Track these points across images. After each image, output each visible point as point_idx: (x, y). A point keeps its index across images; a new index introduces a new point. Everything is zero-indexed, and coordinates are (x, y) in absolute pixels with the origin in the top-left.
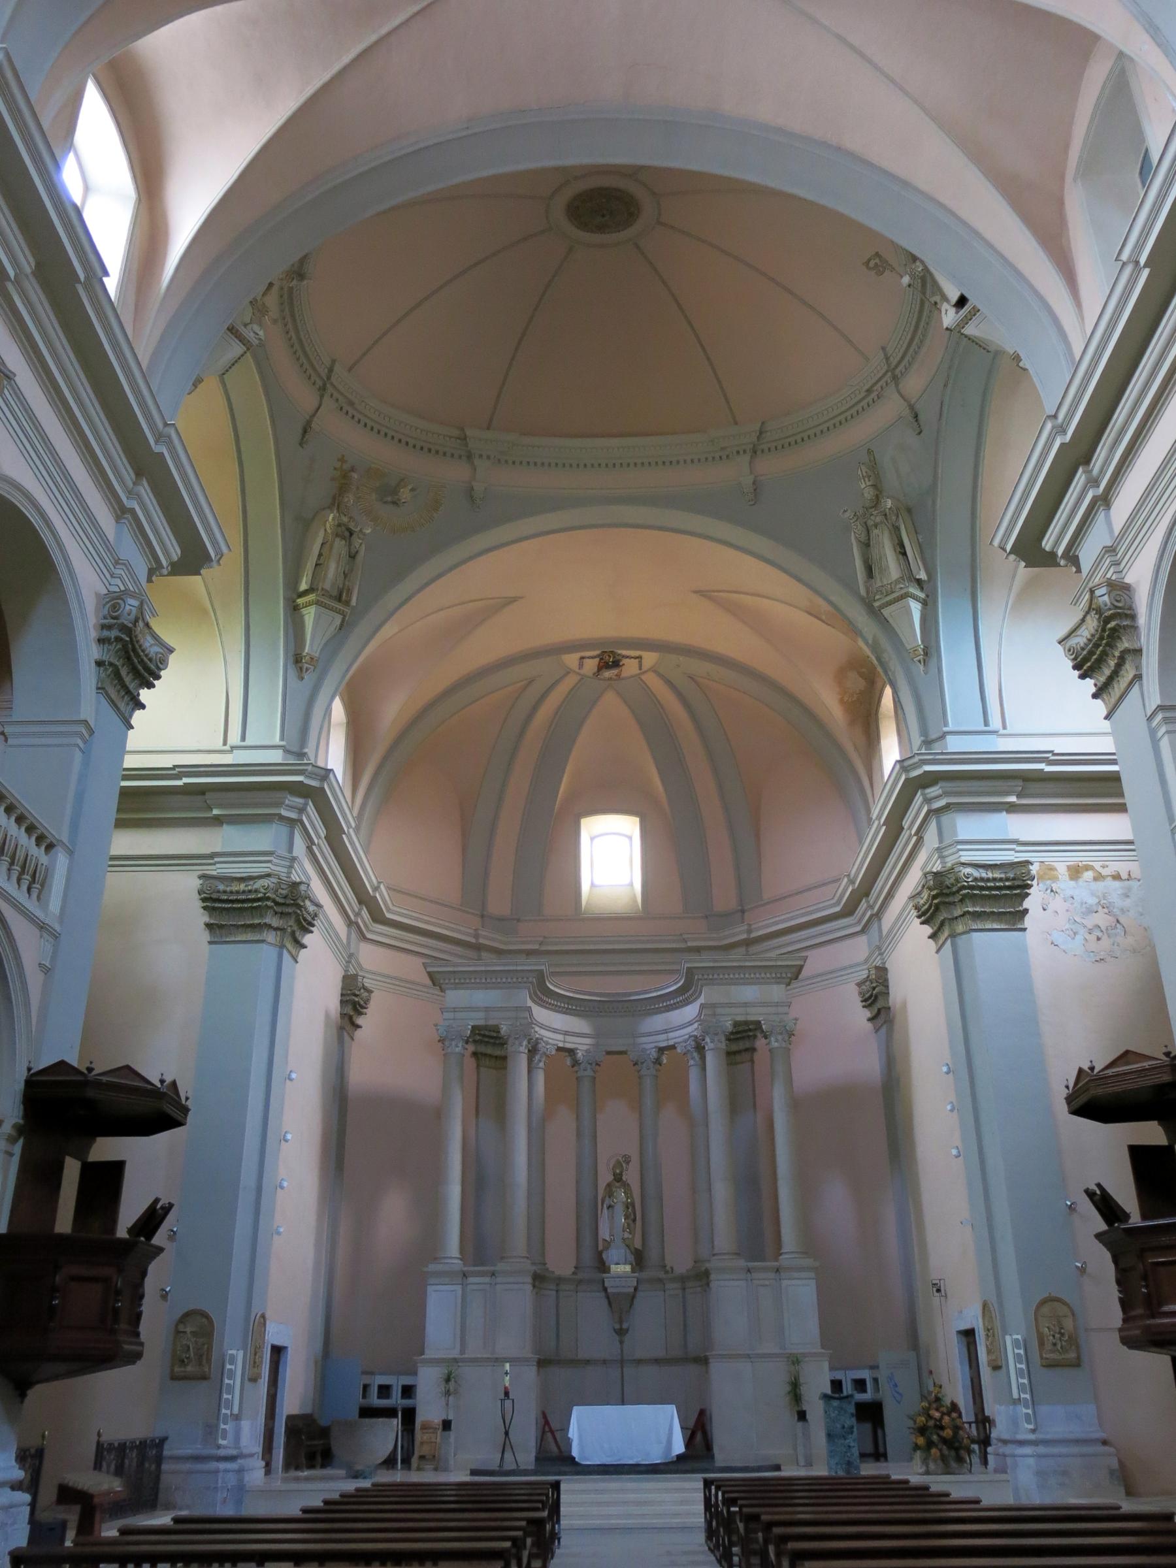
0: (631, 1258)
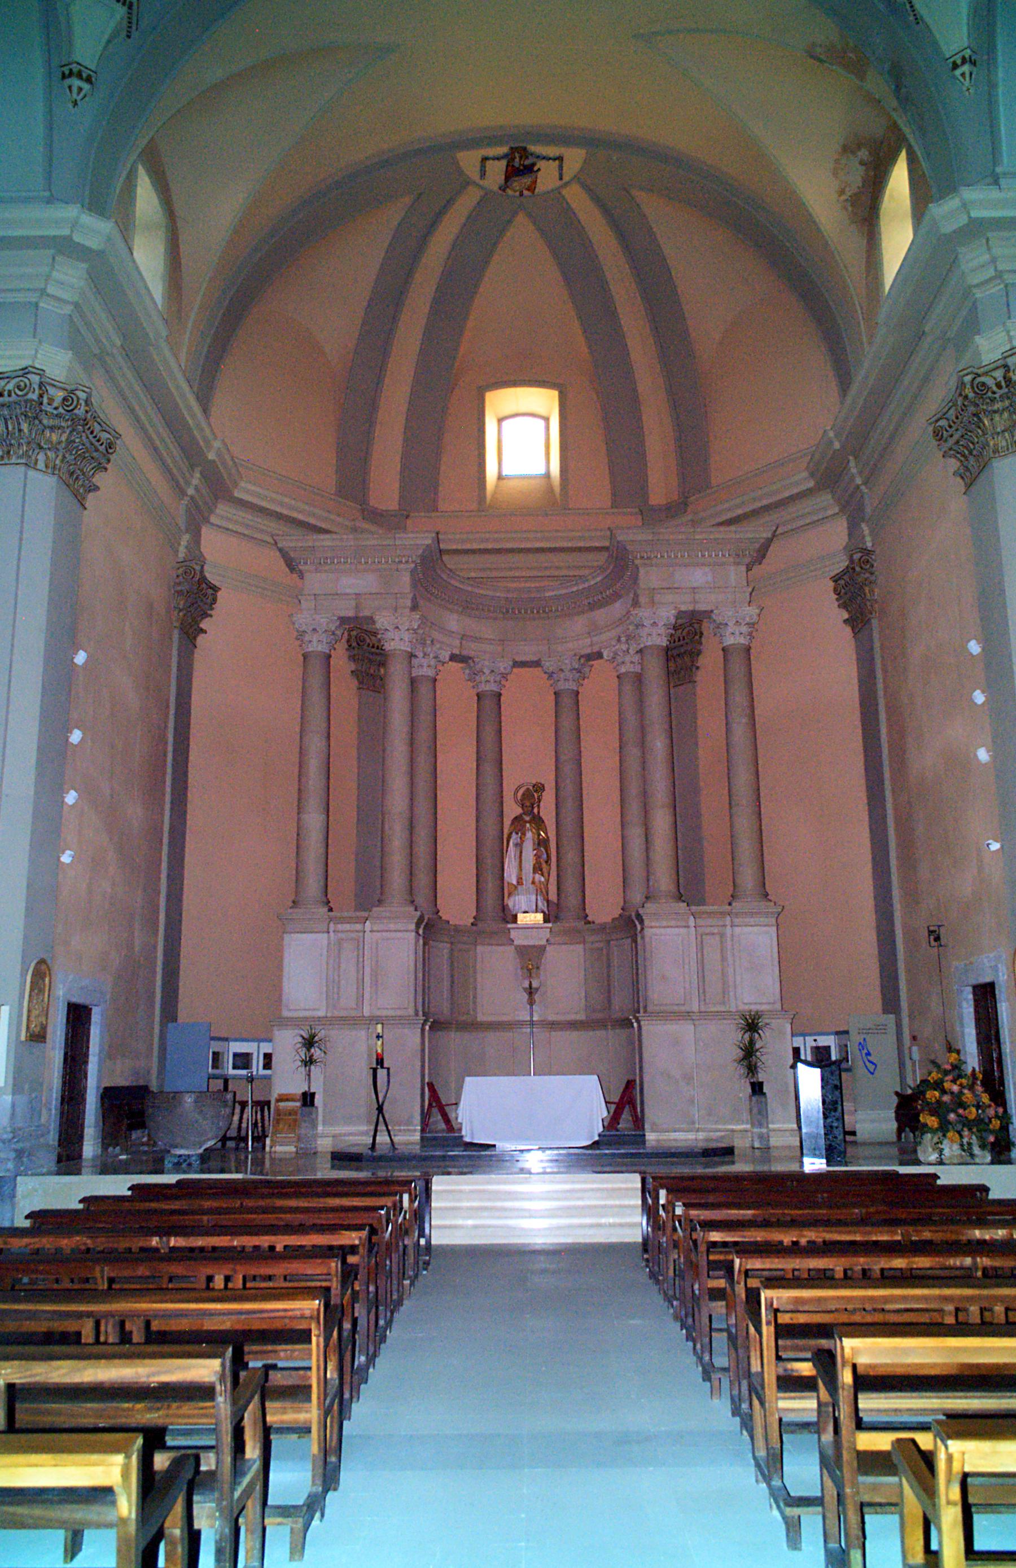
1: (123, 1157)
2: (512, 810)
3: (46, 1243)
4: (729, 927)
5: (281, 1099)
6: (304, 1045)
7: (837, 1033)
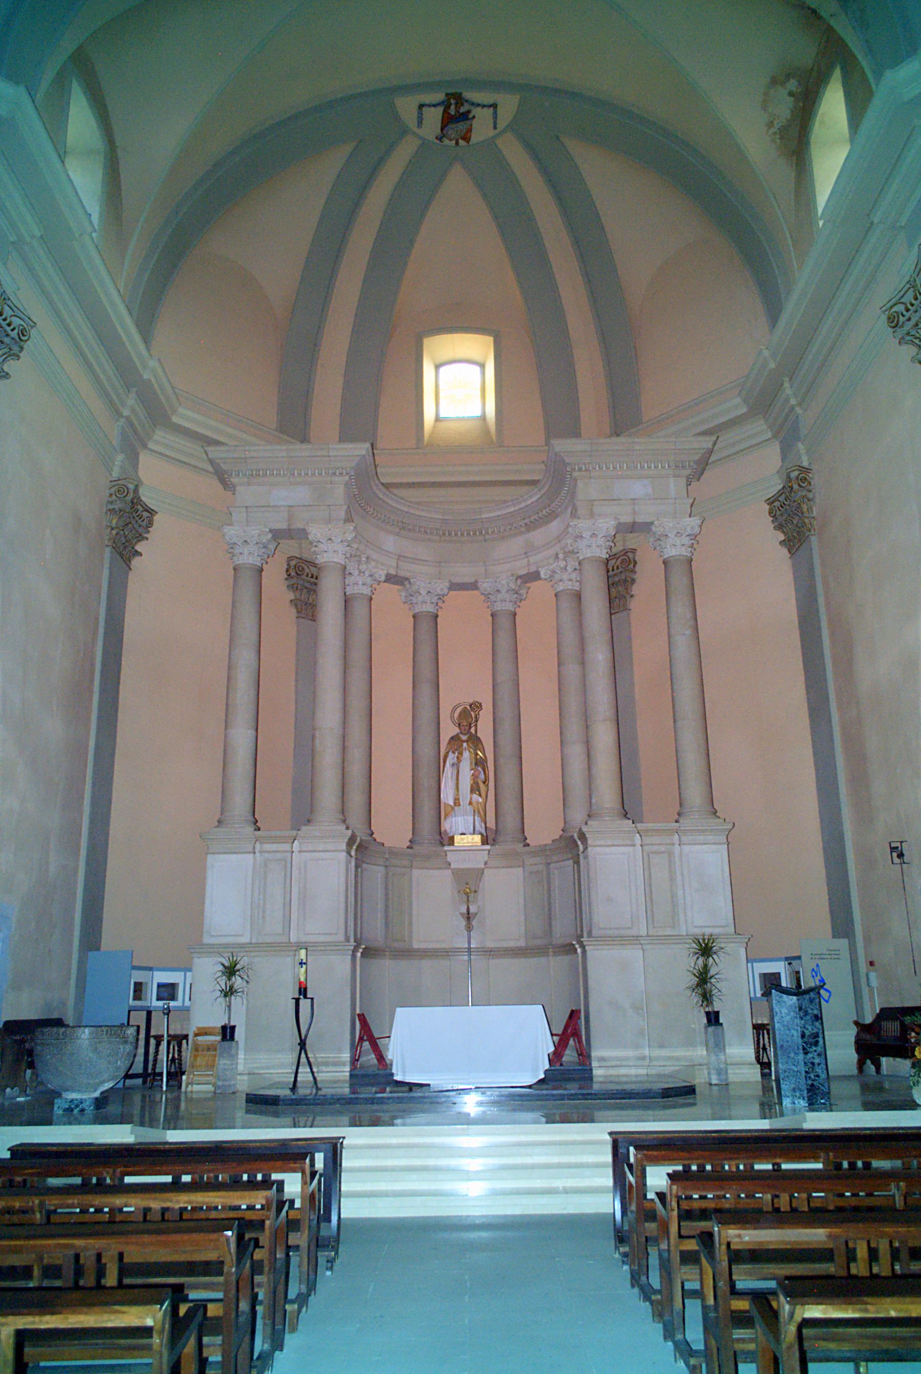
0: (480, 826)
2: (449, 730)
4: (677, 846)
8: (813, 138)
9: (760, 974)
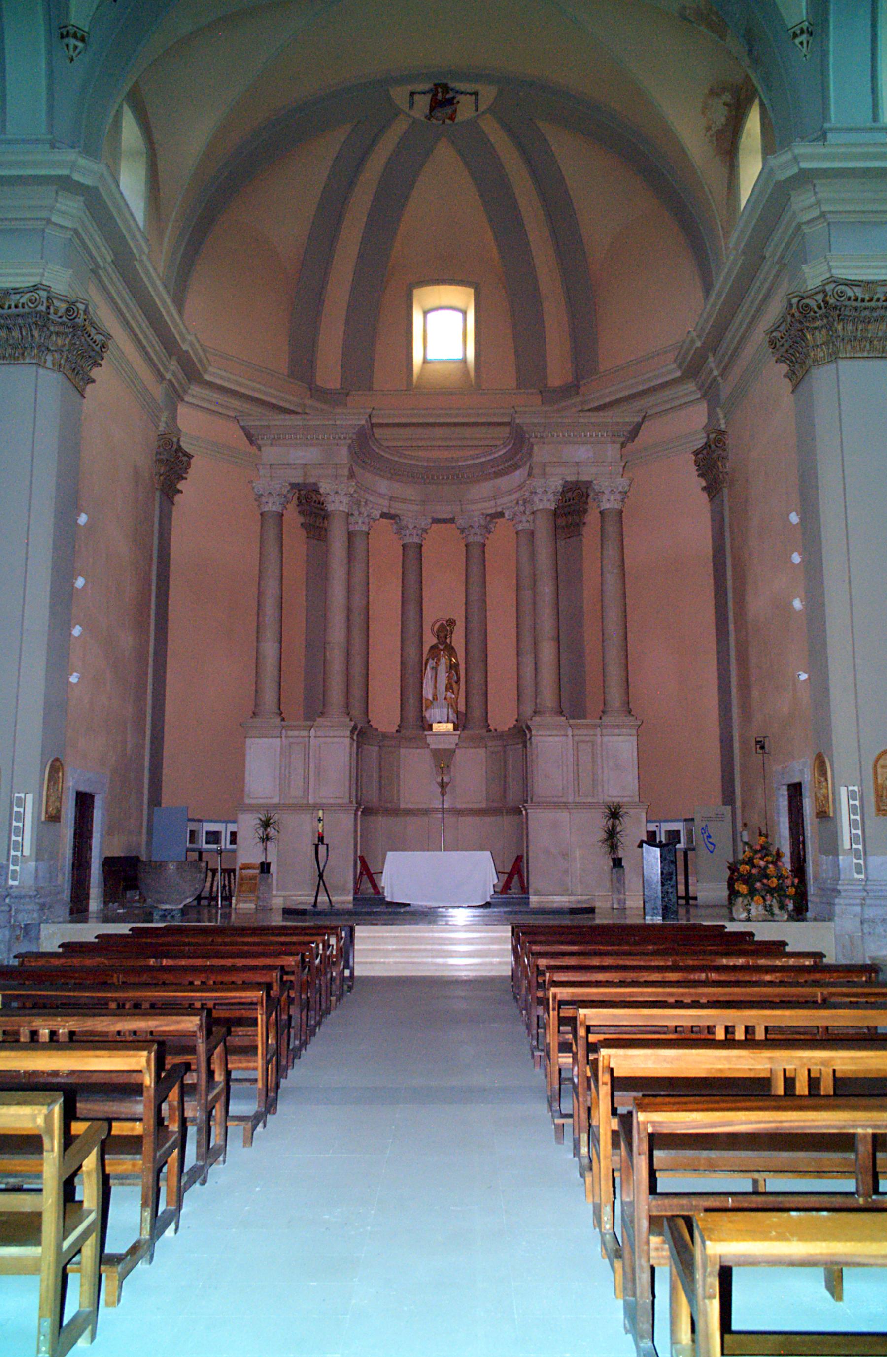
0: (452, 716)
1: (121, 911)
2: (430, 640)
3: (76, 962)
5: (245, 867)
6: (262, 826)
7: (686, 820)
8: (741, 146)
9: (666, 831)
